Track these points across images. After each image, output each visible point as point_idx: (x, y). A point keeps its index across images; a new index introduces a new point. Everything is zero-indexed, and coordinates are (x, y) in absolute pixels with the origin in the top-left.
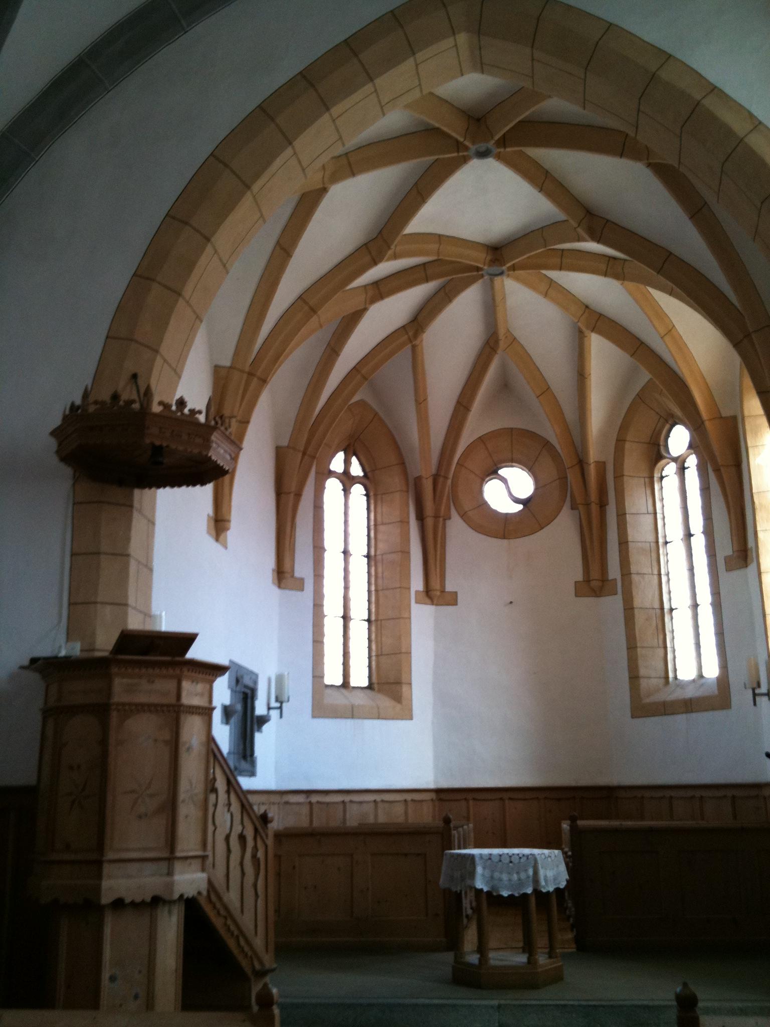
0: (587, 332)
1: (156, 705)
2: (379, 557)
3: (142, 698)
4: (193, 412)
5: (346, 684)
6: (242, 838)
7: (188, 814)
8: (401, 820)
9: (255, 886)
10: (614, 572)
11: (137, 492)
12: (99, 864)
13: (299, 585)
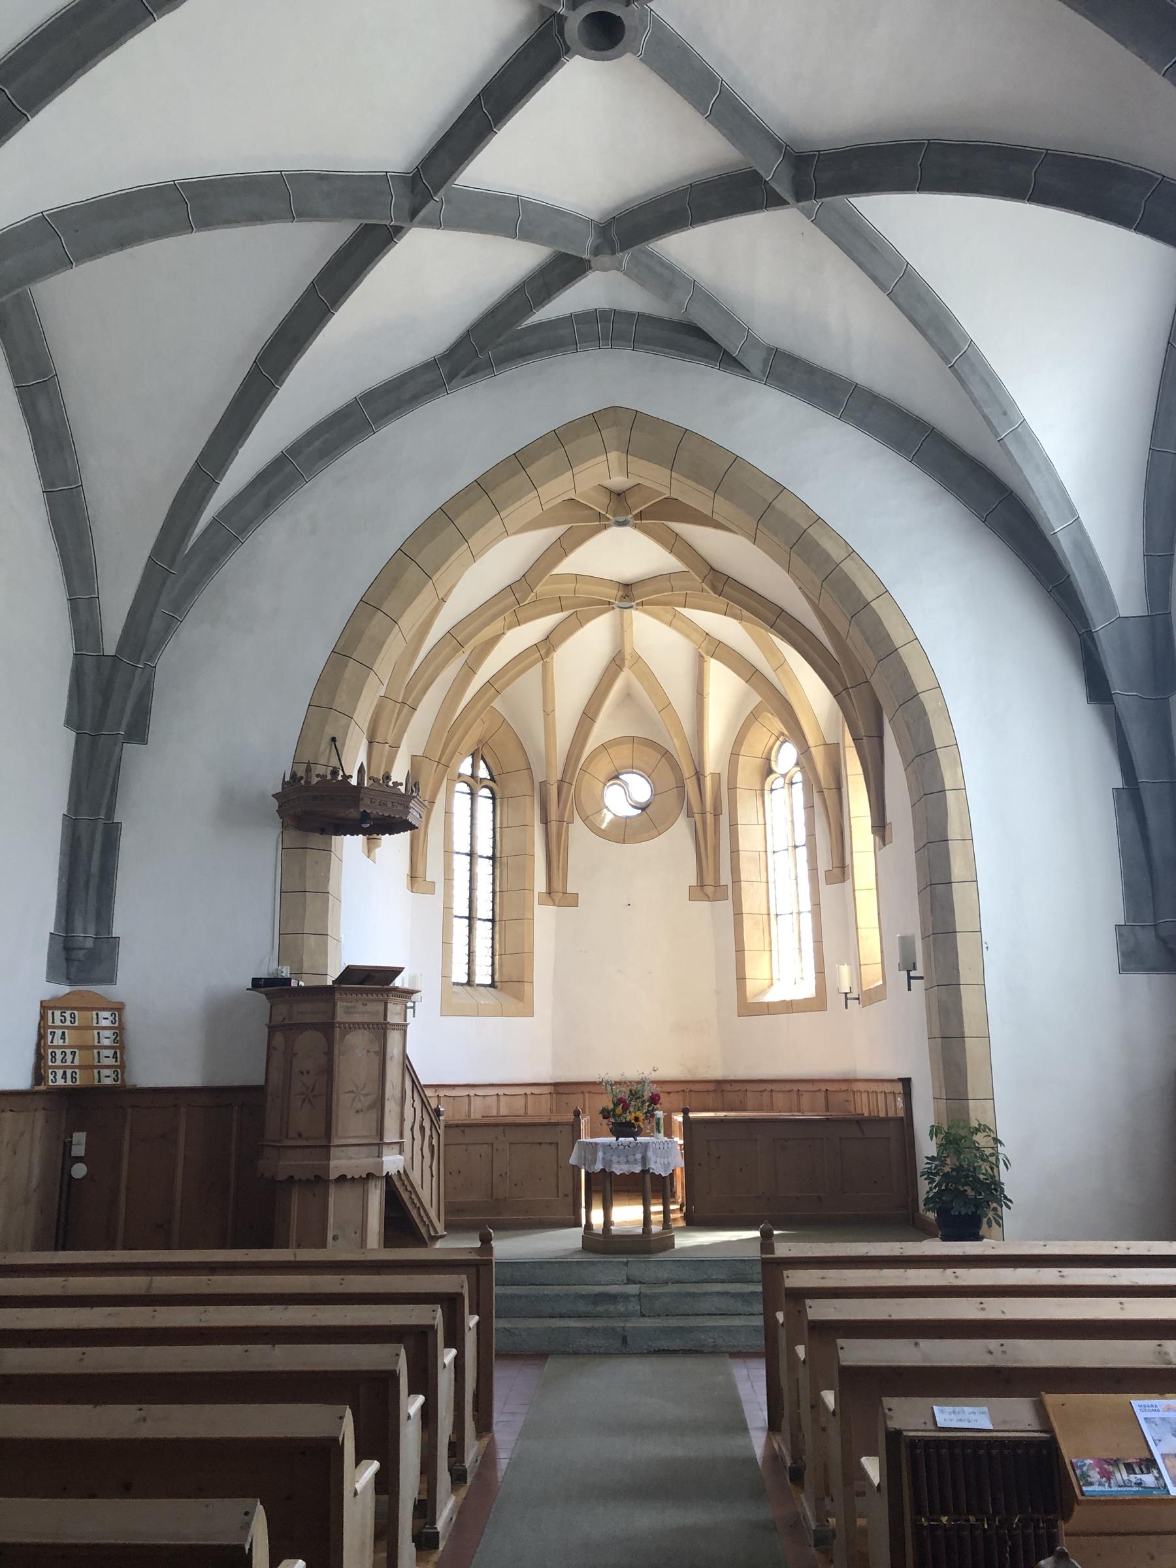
0: (707, 658)
1: (368, 1024)
2: (504, 860)
3: (357, 1018)
4: (396, 784)
5: (470, 983)
6: (422, 1128)
7: (391, 1107)
8: (521, 1112)
9: (431, 1167)
10: (725, 878)
11: (334, 837)
12: (327, 1148)
13: (430, 889)
